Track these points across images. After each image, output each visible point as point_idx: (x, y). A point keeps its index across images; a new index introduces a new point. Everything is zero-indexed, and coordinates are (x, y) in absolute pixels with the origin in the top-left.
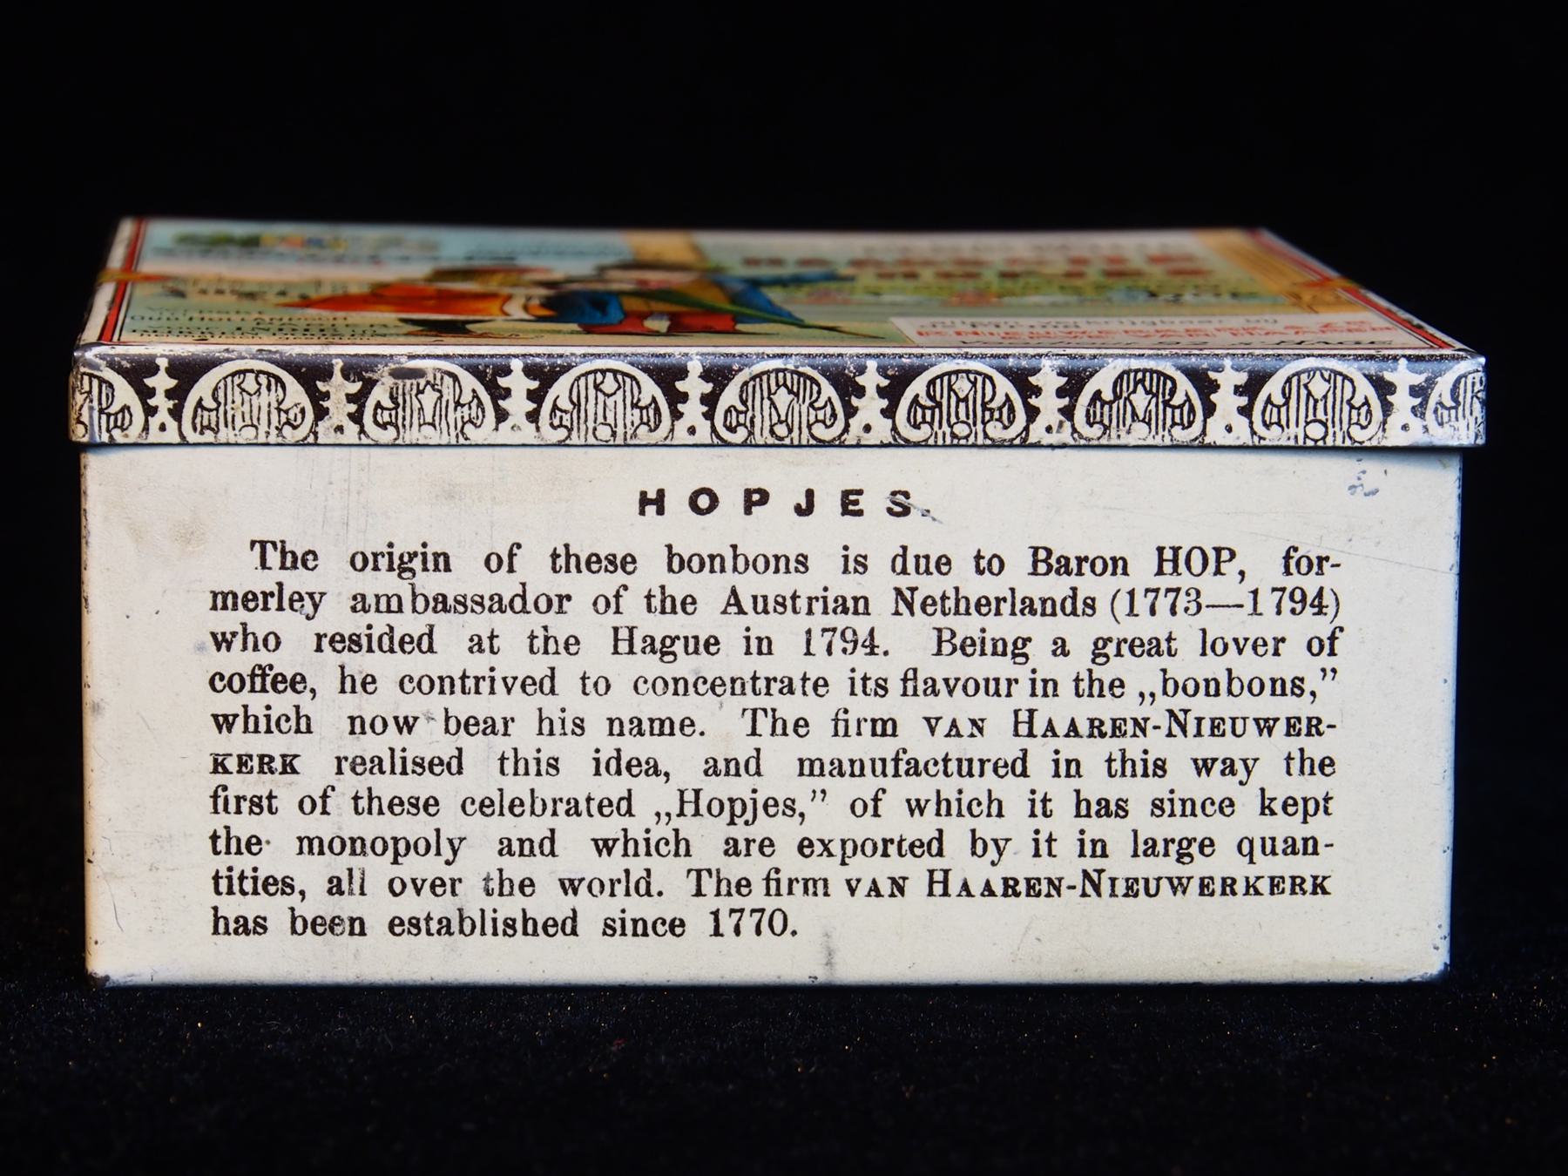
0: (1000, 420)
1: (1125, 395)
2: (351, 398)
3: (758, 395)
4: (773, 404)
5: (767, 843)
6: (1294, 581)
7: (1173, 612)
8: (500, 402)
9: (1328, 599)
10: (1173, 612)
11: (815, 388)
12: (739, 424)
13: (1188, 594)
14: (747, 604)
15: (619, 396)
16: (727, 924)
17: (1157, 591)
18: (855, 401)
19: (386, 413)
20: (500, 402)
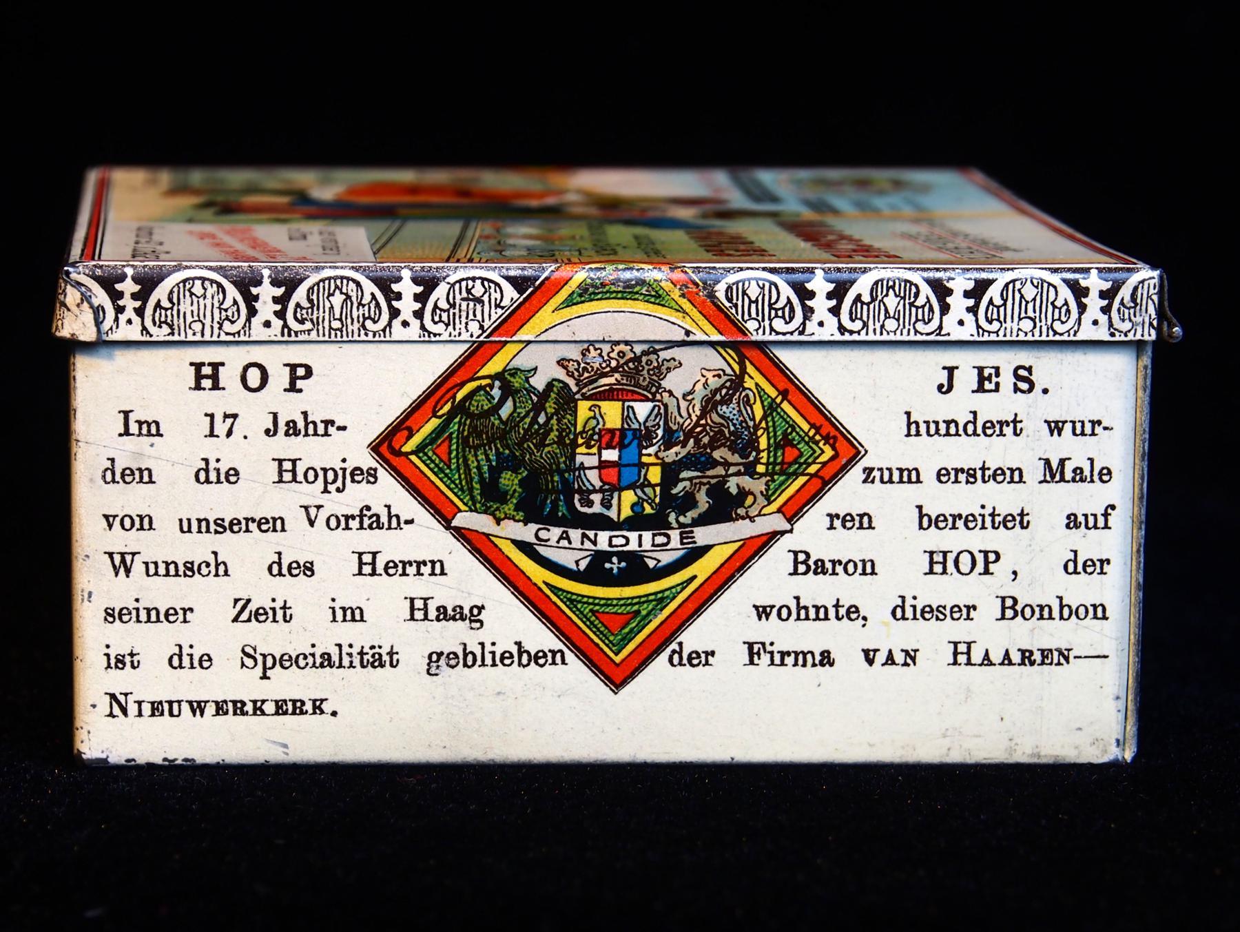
0: (783, 317)
2: (276, 300)
8: (394, 303)
19: (304, 312)
20: (394, 303)
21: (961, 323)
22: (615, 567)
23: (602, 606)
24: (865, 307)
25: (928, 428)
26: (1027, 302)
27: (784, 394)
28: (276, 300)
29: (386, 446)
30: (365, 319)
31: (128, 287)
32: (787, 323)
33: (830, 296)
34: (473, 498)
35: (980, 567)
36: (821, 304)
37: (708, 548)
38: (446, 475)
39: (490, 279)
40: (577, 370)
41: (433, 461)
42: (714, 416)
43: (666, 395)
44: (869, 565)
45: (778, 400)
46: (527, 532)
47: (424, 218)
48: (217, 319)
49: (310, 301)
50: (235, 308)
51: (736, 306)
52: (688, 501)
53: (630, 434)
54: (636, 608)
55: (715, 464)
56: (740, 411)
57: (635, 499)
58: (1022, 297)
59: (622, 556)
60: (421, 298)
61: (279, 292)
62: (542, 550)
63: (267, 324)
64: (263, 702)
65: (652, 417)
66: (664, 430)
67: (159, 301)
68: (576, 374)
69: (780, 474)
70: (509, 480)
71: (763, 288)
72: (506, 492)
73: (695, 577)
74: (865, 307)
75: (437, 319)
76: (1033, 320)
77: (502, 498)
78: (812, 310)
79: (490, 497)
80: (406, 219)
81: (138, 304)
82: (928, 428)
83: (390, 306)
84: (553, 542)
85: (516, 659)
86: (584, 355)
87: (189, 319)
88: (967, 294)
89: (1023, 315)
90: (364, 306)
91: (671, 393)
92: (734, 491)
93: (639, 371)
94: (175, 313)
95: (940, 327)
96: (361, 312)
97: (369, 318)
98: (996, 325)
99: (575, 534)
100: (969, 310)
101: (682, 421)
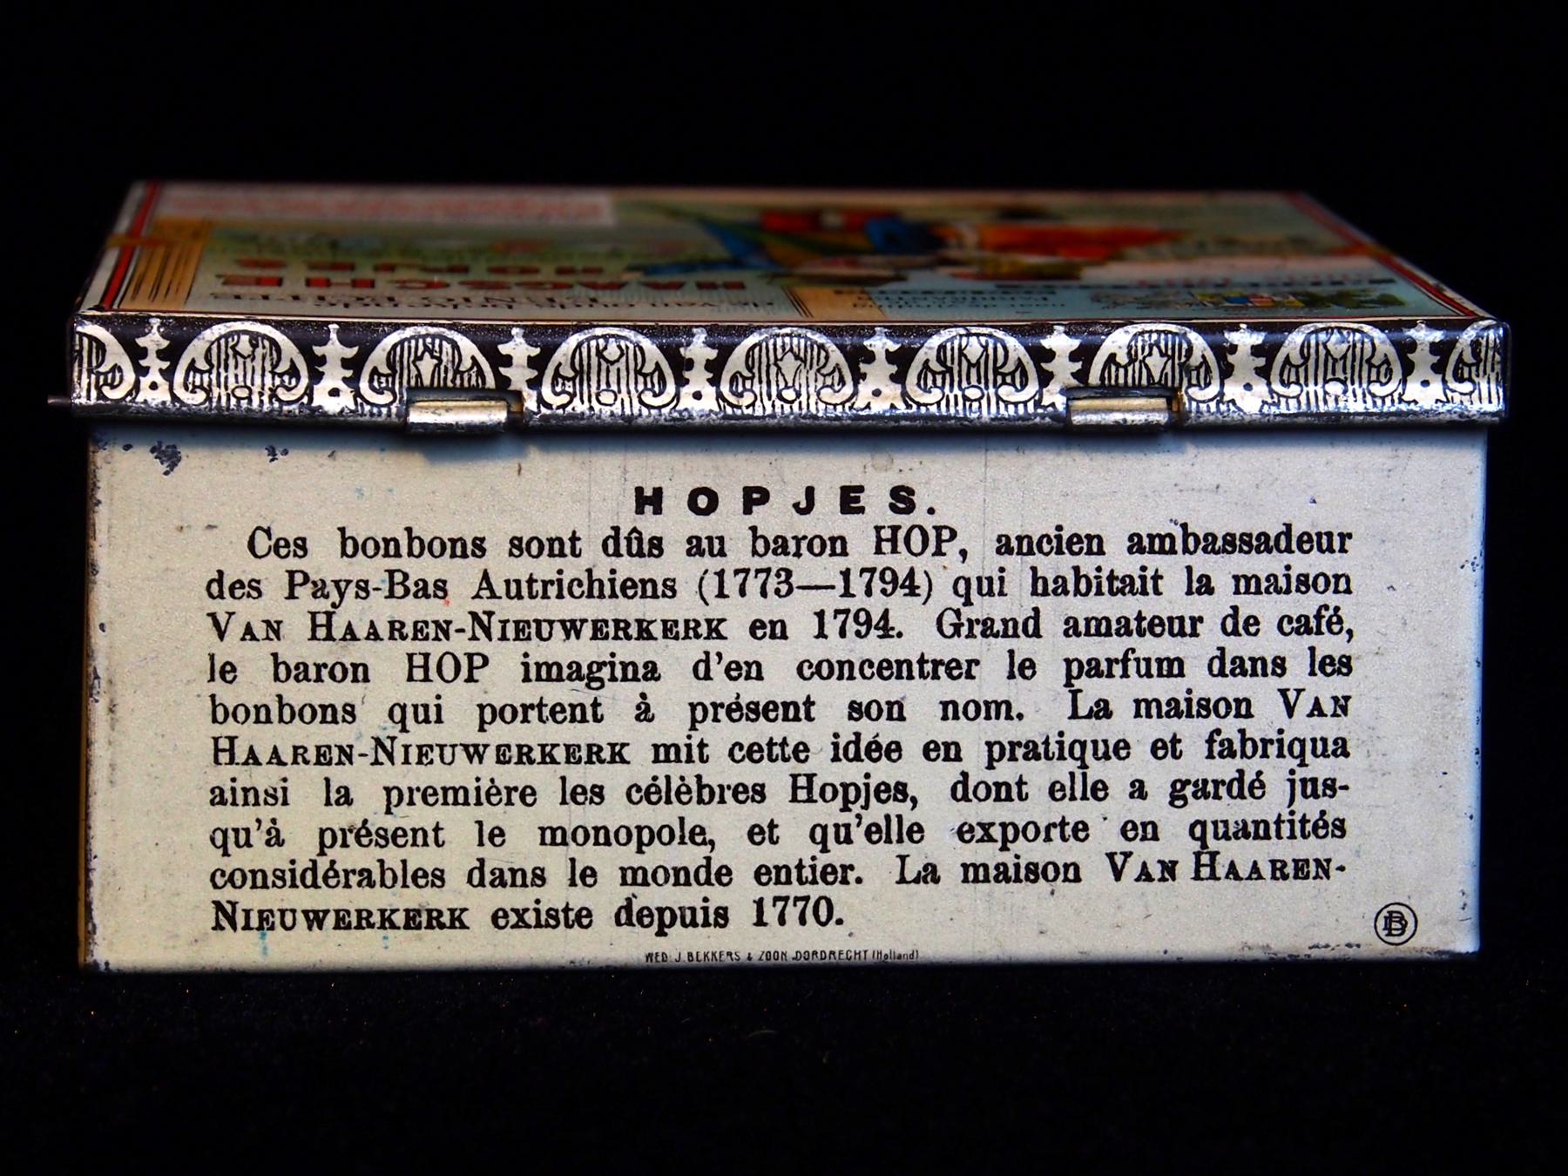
0: (1013, 384)
1: (1140, 357)
2: (346, 363)
3: (764, 359)
4: (779, 369)
5: (529, 791)
6: (887, 560)
7: (764, 594)
8: (502, 370)
9: (920, 580)
10: (764, 594)
11: (823, 354)
12: (745, 390)
13: (778, 575)
14: (500, 589)
15: (622, 364)
16: (771, 914)
17: (747, 571)
18: (863, 367)
19: (383, 379)
20: (502, 370)
25: (237, 838)
26: (1335, 361)
61: (351, 352)
64: (554, 746)
67: (193, 361)
82: (237, 838)
85: (695, 794)
94: (214, 377)
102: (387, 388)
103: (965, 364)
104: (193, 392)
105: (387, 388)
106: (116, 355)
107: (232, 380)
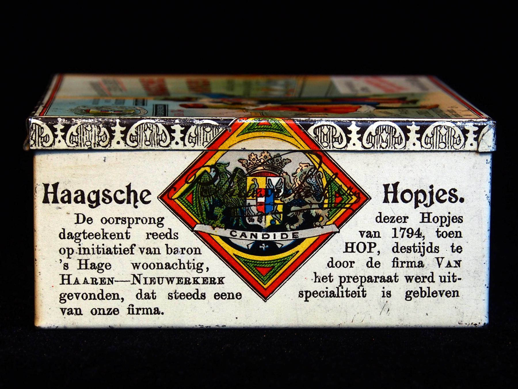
0: (338, 141)
2: (122, 132)
21: (414, 144)
22: (264, 248)
23: (258, 264)
24: (373, 138)
26: (443, 136)
27: (336, 175)
28: (122, 132)
29: (165, 197)
30: (160, 141)
31: (59, 127)
32: (339, 144)
33: (358, 133)
34: (203, 218)
35: (368, 249)
36: (354, 136)
37: (303, 240)
38: (191, 208)
39: (205, 124)
40: (247, 164)
41: (185, 202)
42: (305, 183)
43: (284, 174)
44: (157, 250)
45: (333, 177)
46: (227, 233)
47: (318, 98)
48: (97, 140)
49: (137, 133)
50: (105, 136)
51: (318, 136)
52: (294, 220)
53: (270, 191)
54: (272, 265)
55: (306, 203)
56: (316, 181)
57: (272, 218)
58: (440, 133)
59: (267, 243)
60: (184, 132)
61: (124, 129)
62: (233, 241)
63: (118, 143)
65: (279, 184)
66: (284, 190)
67: (72, 133)
68: (246, 165)
69: (334, 208)
70: (218, 211)
71: (329, 129)
72: (217, 216)
73: (298, 252)
74: (373, 138)
75: (190, 141)
76: (445, 144)
77: (215, 218)
78: (350, 139)
79: (210, 218)
80: (325, 98)
81: (63, 134)
83: (170, 135)
84: (238, 237)
86: (249, 157)
87: (85, 140)
88: (417, 132)
89: (441, 141)
90: (159, 135)
91: (287, 173)
92: (314, 215)
93: (274, 164)
94: (79, 137)
95: (405, 146)
96: (158, 138)
97: (162, 140)
98: (429, 145)
99: (248, 234)
100: (418, 139)
101: (291, 185)
102: (135, 140)
103: (322, 134)
104: (73, 143)
105: (135, 140)
106: (47, 131)
107: (85, 138)
